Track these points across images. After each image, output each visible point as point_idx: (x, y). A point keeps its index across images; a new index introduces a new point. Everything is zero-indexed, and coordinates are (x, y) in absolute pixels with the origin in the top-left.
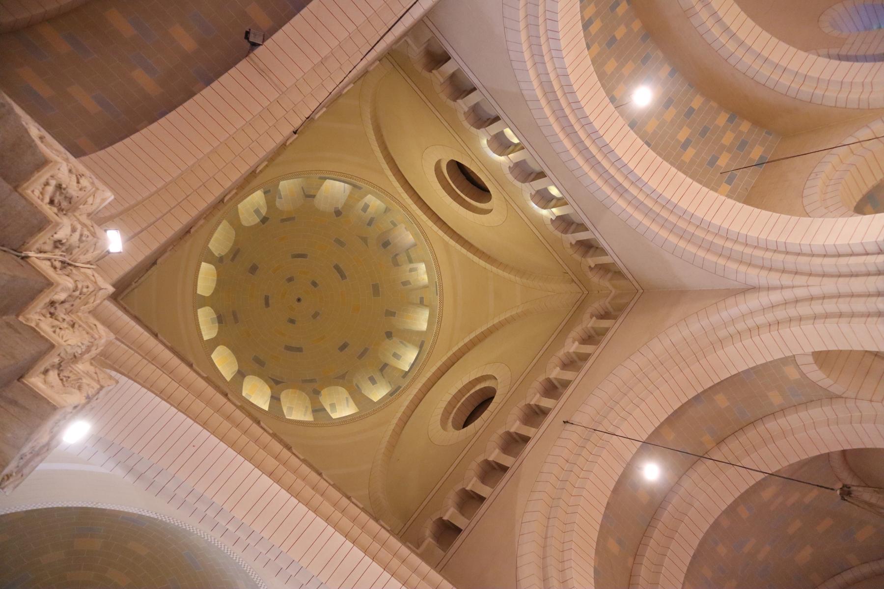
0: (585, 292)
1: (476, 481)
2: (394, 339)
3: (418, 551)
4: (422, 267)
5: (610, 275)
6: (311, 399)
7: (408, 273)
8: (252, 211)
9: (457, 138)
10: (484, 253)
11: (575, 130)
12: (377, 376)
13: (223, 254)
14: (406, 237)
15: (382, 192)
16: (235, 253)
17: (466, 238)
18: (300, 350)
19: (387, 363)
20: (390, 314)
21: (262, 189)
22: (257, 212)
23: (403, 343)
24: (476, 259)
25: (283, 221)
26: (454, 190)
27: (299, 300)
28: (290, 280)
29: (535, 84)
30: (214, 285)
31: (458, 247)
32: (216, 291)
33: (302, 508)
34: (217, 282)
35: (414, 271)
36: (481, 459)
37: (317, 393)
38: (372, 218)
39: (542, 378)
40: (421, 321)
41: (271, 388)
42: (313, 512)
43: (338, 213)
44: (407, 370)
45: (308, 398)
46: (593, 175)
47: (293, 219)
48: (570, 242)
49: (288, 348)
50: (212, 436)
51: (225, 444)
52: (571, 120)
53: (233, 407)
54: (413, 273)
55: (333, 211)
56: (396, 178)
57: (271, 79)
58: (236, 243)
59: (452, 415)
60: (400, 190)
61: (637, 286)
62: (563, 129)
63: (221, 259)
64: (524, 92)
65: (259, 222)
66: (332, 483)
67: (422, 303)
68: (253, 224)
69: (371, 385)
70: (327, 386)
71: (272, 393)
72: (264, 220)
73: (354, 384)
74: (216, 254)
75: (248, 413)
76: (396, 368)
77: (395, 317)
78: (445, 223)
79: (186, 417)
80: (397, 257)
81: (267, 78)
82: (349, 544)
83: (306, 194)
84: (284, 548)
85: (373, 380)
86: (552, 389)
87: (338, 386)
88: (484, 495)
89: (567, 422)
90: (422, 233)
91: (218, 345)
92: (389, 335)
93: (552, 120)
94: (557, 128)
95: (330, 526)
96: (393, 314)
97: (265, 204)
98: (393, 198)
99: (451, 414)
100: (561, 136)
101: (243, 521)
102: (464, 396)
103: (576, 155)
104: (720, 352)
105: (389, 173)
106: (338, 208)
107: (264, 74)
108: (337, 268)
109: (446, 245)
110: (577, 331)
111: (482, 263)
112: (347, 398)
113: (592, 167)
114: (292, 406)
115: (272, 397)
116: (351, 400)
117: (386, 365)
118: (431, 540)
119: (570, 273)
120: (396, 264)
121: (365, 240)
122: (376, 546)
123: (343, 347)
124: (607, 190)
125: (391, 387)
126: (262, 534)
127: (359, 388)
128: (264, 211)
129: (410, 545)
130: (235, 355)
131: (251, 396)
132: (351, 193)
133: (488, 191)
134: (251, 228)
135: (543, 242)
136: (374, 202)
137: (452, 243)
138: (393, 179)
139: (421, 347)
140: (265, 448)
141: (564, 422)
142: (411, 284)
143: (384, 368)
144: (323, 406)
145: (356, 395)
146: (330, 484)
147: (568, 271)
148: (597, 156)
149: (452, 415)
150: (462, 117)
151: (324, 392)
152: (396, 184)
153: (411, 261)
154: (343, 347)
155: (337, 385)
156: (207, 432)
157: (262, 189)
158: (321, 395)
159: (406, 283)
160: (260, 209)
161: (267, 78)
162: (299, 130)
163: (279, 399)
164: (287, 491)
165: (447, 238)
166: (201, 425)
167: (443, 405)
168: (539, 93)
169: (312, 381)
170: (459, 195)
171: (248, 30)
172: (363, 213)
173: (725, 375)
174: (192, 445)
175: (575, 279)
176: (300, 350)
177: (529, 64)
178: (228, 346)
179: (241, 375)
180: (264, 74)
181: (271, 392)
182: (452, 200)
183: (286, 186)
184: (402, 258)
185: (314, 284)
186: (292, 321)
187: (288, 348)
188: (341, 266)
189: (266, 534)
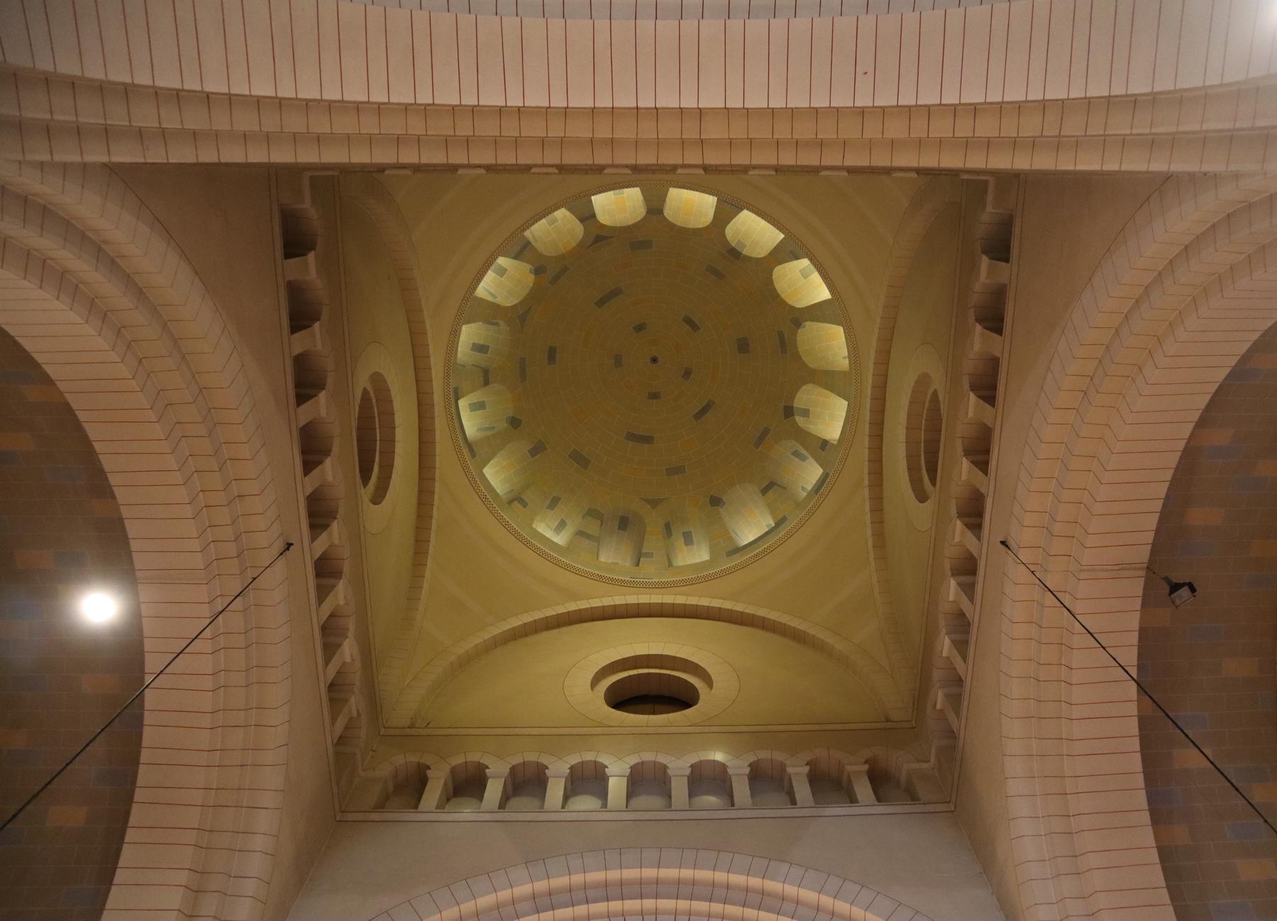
0: (383, 729)
1: (315, 346)
2: (505, 425)
3: (308, 174)
4: (560, 539)
5: (391, 789)
6: (541, 256)
7: (764, 524)
8: (811, 409)
9: (752, 729)
10: (526, 636)
11: (694, 900)
12: (479, 358)
13: (800, 331)
14: (613, 555)
15: (700, 577)
16: (785, 344)
17: (564, 629)
18: (601, 302)
19: (486, 387)
20: (536, 450)
21: (836, 443)
22: (806, 413)
23: (488, 429)
24: (528, 618)
25: (766, 432)
26: (661, 668)
27: (654, 360)
28: (687, 373)
29: (791, 890)
30: (777, 286)
31: (561, 609)
32: (769, 281)
33: (929, 98)
34: (777, 293)
35: (557, 526)
36: (330, 381)
37: (538, 271)
38: (672, 535)
39: (347, 568)
40: (497, 475)
41: (602, 226)
42: (839, 108)
43: (716, 502)
44: (459, 402)
45: (545, 254)
46: (597, 876)
47: (757, 445)
48: (431, 767)
49: (616, 293)
50: (1000, 100)
51: (625, 108)
52: (699, 902)
53: (827, 162)
54: (557, 524)
55: (724, 499)
56: (737, 611)
57: (1107, 570)
58: (797, 357)
59: (374, 401)
60: (692, 601)
61: (350, 817)
62: (694, 882)
63: (797, 323)
64: (786, 866)
65: (793, 403)
66: (679, 171)
67: (516, 499)
68: (799, 395)
69: (476, 342)
70: (533, 288)
71: (597, 220)
72: (789, 412)
73: (501, 323)
74: (808, 323)
75: (719, 171)
76: (472, 391)
77: (529, 451)
78: (604, 619)
79: (1128, 93)
80: (599, 521)
81: (1110, 567)
82: (734, 103)
83: (776, 487)
84: (867, 21)
85: (480, 348)
86: (326, 570)
87: (520, 302)
88: (296, 335)
89: (288, 549)
90: (612, 580)
91: (712, 223)
92: (514, 422)
93: (720, 876)
94: (704, 875)
95: (694, 108)
96: (535, 451)
97: (808, 430)
98: (689, 583)
99: (377, 401)
100: (687, 873)
101: (962, 9)
102: (380, 440)
103: (765, 884)
104: (183, 877)
105: (727, 605)
106: (722, 508)
107: (1115, 567)
108: (648, 440)
109: (574, 597)
110: (357, 678)
111: (516, 622)
112: (496, 298)
113: (606, 884)
114: (553, 226)
115: (593, 216)
116: (490, 299)
117: (486, 383)
118: (302, 206)
119: (422, 732)
120: (592, 513)
121: (654, 503)
122: (603, 132)
123: (552, 355)
124: (559, 882)
125: (459, 364)
126: (872, 17)
127: (492, 324)
128: (799, 420)
129: (331, 173)
130: (620, 227)
131: (614, 195)
132: (731, 539)
133: (613, 707)
134: (797, 389)
135: (517, 729)
136: (696, 555)
137: (572, 606)
138: (716, 603)
139: (470, 446)
140: (920, 143)
141: (290, 545)
142: (547, 508)
143: (486, 377)
144: (520, 260)
145: (491, 313)
146: (684, 166)
147: (427, 731)
148: (653, 901)
149: (374, 401)
150: (779, 756)
151: (531, 279)
152: (705, 602)
153: (580, 533)
154: (552, 355)
155: (521, 303)
156: (1035, 98)
157: (836, 443)
158: (531, 272)
159: (554, 503)
160: (805, 418)
161: (1110, 567)
162: (1009, 552)
163: (582, 220)
164: (928, 107)
165: (583, 605)
166: (1093, 98)
167: (397, 404)
168: (772, 886)
169: (556, 278)
170: (636, 668)
171: (1195, 594)
172: (684, 531)
173: (128, 855)
174: (871, 72)
175: (413, 732)
176: (601, 302)
177: (826, 901)
178: (697, 232)
179: (655, 208)
180: (1115, 567)
181: (599, 222)
182: (651, 653)
183: (811, 473)
184: (593, 527)
185: (654, 396)
186: (640, 328)
187: (616, 293)
188: (646, 445)
189: (867, 21)
